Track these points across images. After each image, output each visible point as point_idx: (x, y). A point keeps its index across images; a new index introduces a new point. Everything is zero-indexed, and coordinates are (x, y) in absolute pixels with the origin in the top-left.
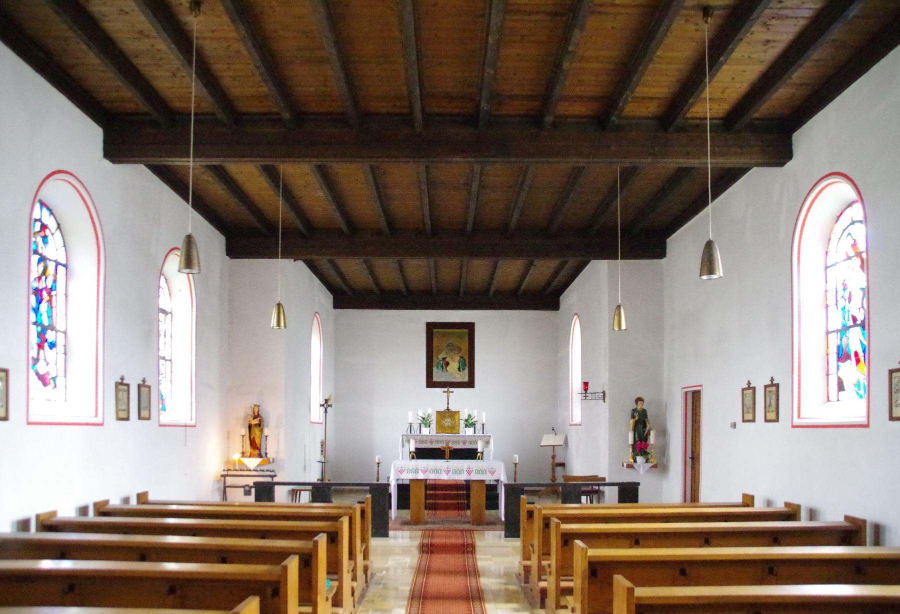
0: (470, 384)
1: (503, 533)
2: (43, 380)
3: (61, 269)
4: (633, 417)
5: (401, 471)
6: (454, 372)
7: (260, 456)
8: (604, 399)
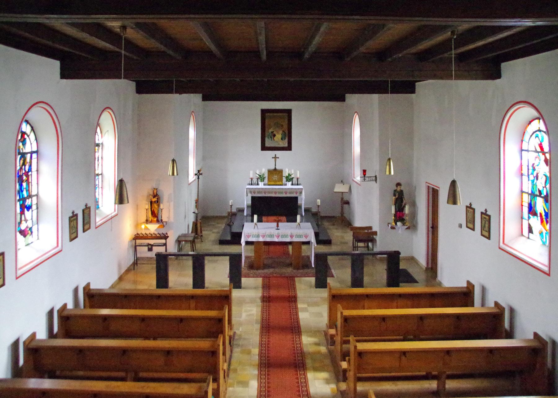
0: (289, 148)
1: (313, 280)
2: (24, 233)
3: (34, 155)
4: (395, 195)
5: (248, 236)
6: (278, 140)
7: (158, 221)
8: (376, 181)
